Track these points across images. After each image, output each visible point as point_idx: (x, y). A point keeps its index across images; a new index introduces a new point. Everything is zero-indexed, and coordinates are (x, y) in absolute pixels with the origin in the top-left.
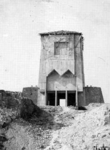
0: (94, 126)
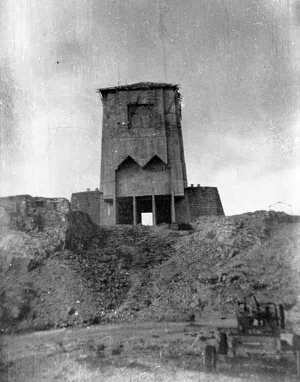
0: (213, 260)
